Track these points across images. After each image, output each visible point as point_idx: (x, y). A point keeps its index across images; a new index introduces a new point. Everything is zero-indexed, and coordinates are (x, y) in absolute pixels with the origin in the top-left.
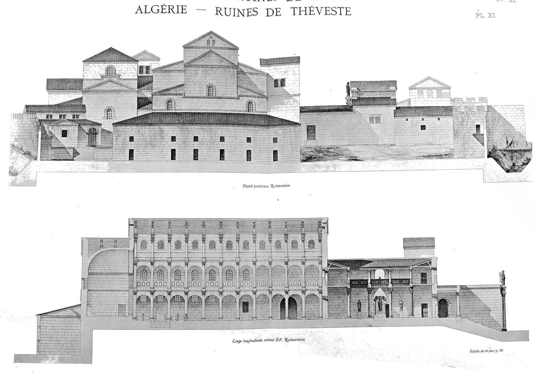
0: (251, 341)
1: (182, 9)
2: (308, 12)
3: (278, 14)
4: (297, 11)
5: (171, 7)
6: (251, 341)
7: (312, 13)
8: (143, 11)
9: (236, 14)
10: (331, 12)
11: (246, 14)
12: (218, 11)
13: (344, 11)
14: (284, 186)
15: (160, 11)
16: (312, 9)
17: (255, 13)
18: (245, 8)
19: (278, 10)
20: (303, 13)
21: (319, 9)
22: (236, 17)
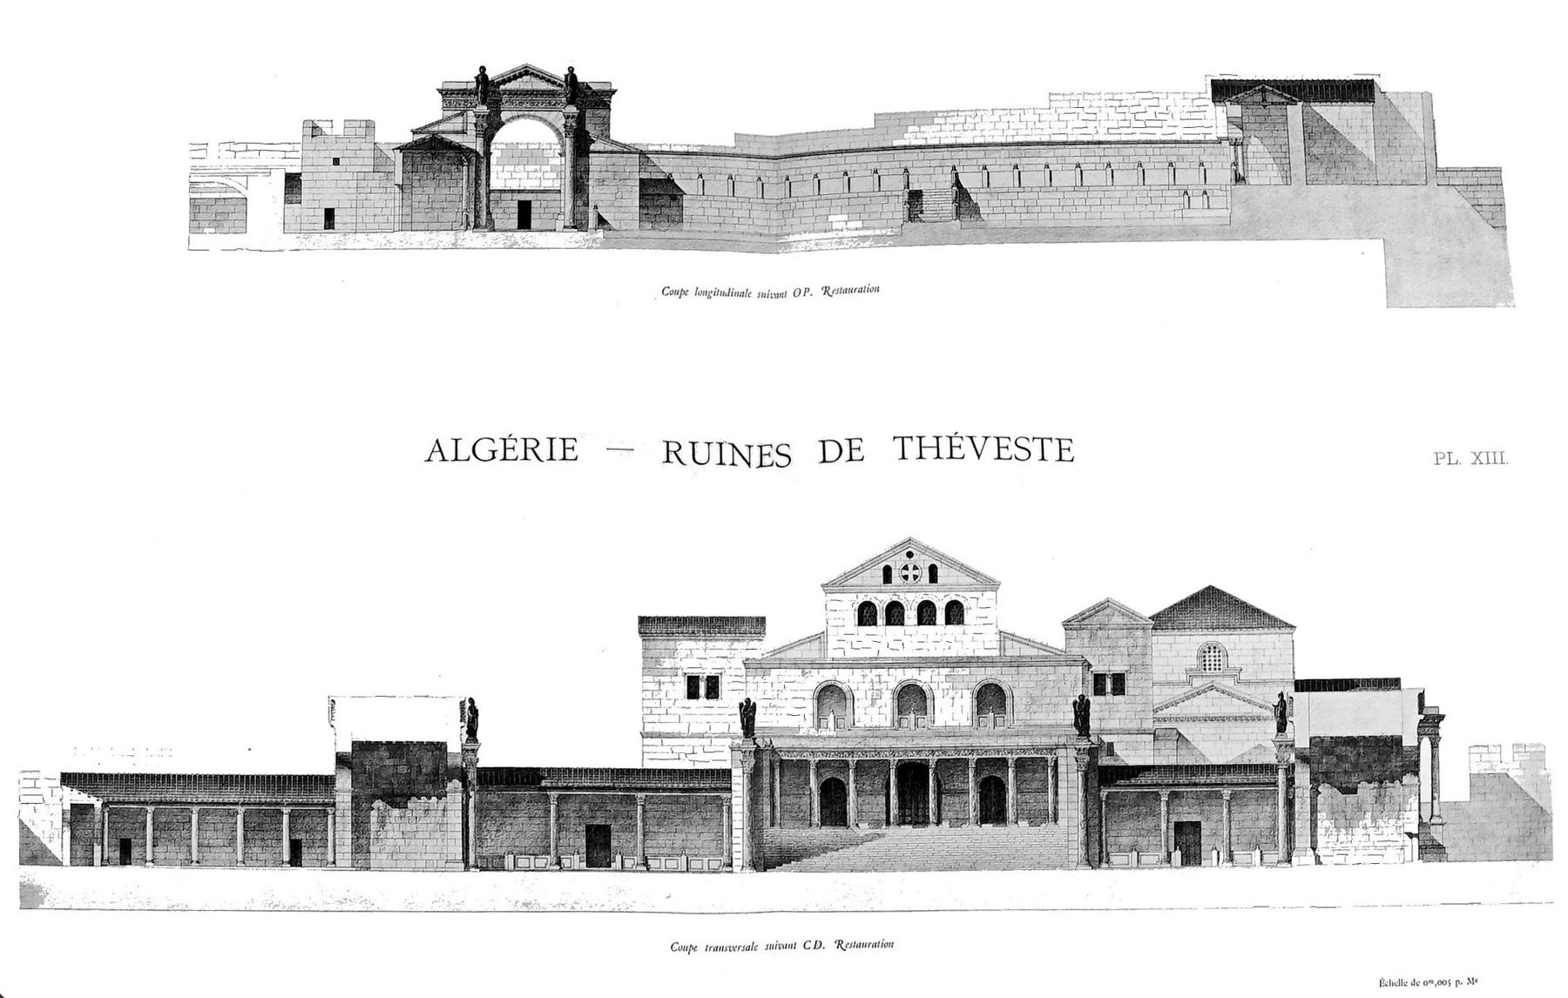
0: (717, 293)
1: (564, 449)
2: (945, 452)
3: (856, 455)
4: (912, 448)
5: (531, 444)
6: (717, 293)
7: (956, 453)
8: (450, 454)
9: (727, 459)
10: (1014, 450)
11: (755, 461)
12: (671, 453)
13: (1052, 450)
14: (875, 945)
15: (499, 455)
16: (956, 442)
17: (784, 461)
18: (755, 443)
19: (855, 444)
20: (929, 453)
21: (979, 442)
22: (727, 468)
